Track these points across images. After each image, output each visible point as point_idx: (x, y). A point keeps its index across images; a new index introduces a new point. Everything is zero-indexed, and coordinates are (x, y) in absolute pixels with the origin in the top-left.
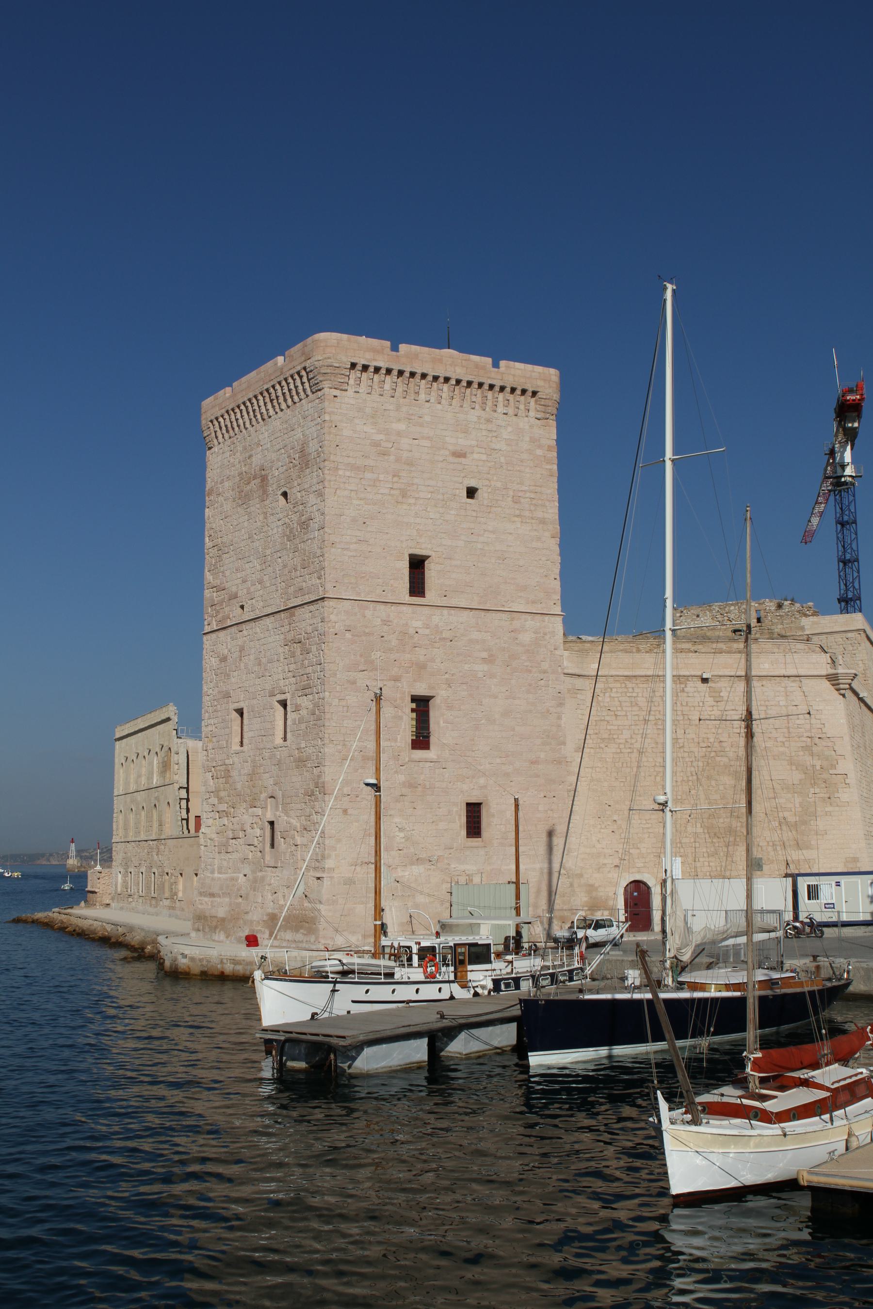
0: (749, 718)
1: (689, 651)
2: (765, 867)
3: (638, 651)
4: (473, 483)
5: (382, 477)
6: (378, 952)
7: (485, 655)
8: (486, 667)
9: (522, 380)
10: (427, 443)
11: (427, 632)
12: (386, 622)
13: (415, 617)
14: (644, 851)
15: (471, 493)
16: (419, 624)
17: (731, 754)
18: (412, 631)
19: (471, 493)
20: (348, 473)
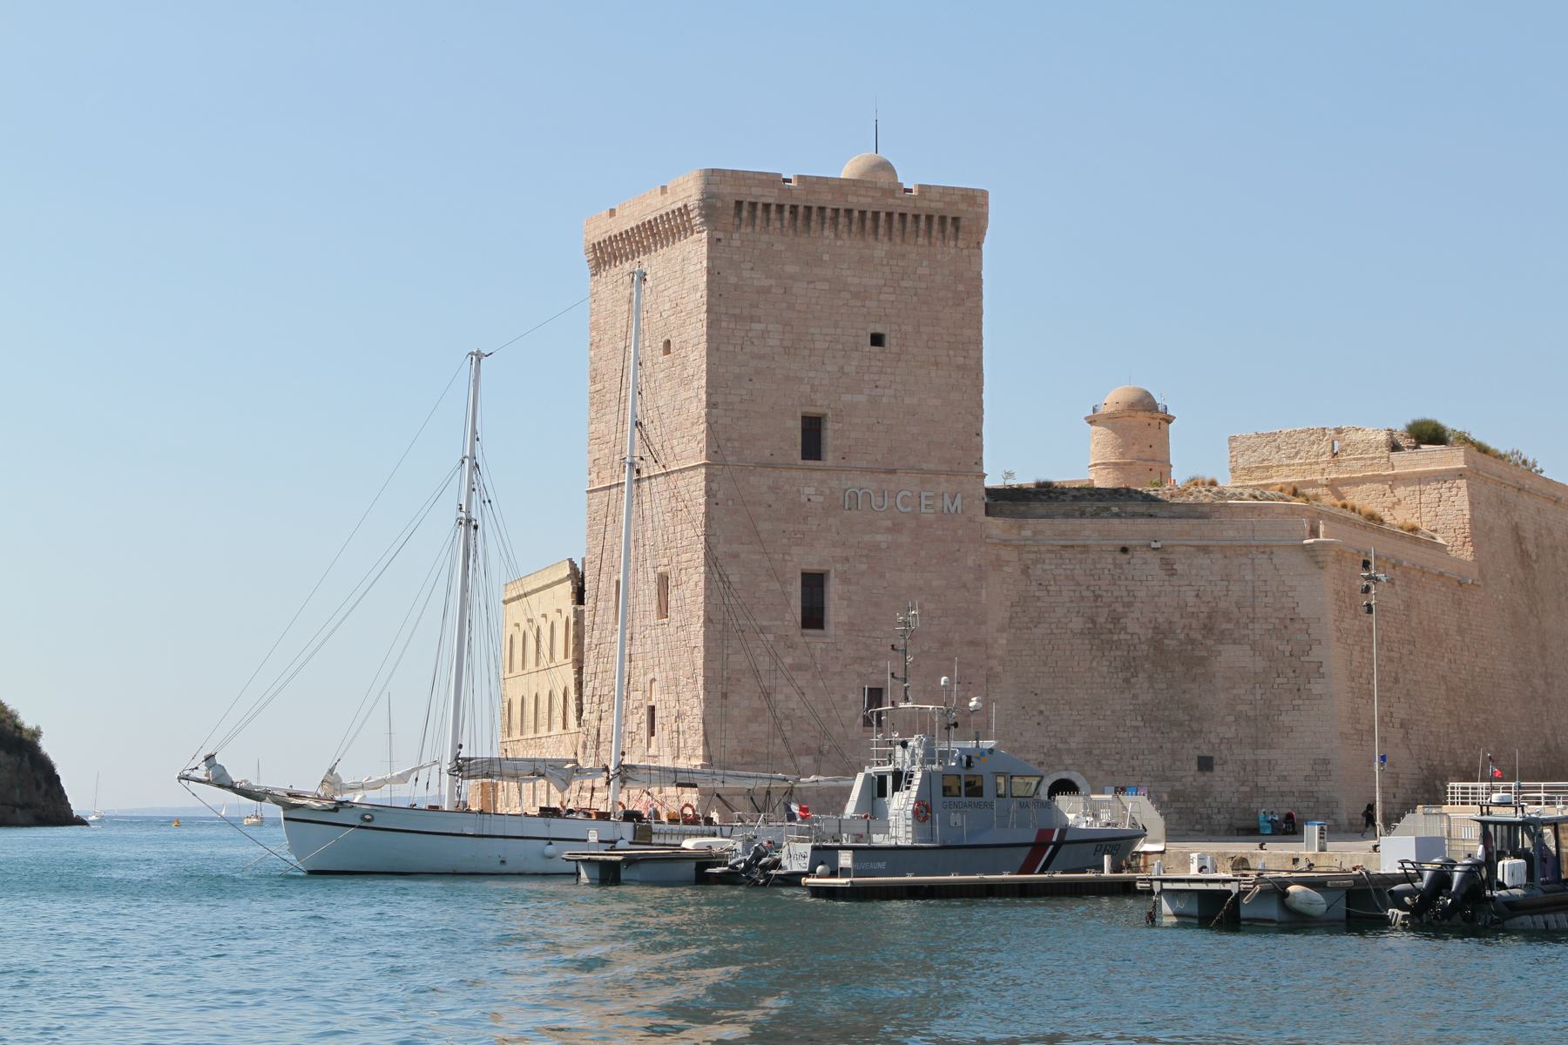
0: (525, 595)
1: (1142, 515)
2: (1216, 768)
3: (1082, 515)
4: (879, 329)
5: (770, 327)
6: (462, 768)
7: (889, 523)
8: (890, 538)
9: (940, 205)
10: (826, 286)
11: (821, 499)
12: (773, 489)
13: (810, 484)
14: (1073, 746)
15: (877, 340)
16: (809, 491)
17: (1182, 637)
18: (804, 499)
19: (877, 340)
20: (732, 325)
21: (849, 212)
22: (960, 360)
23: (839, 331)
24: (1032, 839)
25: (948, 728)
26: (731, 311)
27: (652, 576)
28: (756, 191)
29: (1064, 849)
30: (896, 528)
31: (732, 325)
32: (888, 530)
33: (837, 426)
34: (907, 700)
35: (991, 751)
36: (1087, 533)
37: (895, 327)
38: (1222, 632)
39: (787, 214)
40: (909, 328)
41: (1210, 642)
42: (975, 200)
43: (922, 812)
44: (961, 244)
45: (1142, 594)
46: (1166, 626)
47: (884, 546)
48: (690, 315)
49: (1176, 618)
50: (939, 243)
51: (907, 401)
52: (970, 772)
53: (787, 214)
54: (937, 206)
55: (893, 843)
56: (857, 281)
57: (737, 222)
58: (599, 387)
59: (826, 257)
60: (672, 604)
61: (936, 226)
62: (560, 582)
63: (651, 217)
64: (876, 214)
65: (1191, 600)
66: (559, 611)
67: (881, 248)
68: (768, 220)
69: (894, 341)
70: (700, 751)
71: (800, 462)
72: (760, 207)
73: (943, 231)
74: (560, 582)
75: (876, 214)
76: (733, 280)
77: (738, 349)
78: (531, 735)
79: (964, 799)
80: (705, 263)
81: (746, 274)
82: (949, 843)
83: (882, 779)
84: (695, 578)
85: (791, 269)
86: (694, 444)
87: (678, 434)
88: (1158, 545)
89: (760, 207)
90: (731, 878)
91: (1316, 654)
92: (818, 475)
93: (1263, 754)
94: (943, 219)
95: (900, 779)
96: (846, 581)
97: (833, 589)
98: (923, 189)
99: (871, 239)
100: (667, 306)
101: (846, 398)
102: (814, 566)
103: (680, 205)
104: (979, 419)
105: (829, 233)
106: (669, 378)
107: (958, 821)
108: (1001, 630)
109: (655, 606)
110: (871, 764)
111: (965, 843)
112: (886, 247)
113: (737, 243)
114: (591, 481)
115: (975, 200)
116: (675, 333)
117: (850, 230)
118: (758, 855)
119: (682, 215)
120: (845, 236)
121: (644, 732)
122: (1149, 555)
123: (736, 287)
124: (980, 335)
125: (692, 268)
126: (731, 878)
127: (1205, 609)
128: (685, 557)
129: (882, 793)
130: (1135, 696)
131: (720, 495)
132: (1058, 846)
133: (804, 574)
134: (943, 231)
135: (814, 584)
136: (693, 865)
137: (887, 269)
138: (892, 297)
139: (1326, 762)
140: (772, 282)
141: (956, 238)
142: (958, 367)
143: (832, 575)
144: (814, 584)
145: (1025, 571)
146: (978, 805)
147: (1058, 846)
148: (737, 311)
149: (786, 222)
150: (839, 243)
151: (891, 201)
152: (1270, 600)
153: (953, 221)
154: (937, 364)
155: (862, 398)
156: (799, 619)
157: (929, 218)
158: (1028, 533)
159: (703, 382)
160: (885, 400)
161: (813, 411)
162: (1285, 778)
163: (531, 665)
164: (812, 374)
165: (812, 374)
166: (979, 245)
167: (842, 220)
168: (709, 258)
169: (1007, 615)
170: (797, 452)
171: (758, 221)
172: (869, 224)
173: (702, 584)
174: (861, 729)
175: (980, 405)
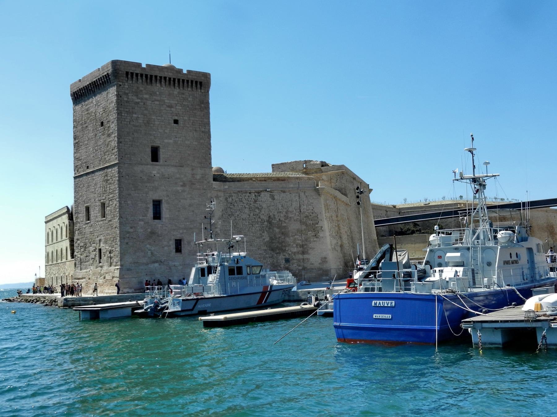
4: (176, 118)
5: (139, 116)
8: (182, 188)
9: (196, 77)
11: (158, 175)
15: (176, 122)
16: (155, 172)
18: (153, 175)
21: (165, 78)
22: (203, 129)
23: (163, 118)
24: (261, 290)
25: (229, 248)
26: (126, 110)
27: (98, 204)
28: (133, 69)
29: (272, 293)
30: (184, 185)
31: (126, 115)
32: (182, 186)
33: (163, 151)
34: (211, 238)
35: (245, 257)
36: (246, 186)
37: (181, 118)
38: (291, 218)
39: (144, 77)
40: (186, 118)
41: (287, 221)
42: (207, 76)
43: (222, 282)
44: (202, 91)
45: (264, 206)
46: (272, 216)
47: (180, 191)
48: (110, 111)
49: (276, 214)
50: (195, 90)
51: (187, 142)
52: (238, 265)
53: (144, 77)
54: (195, 78)
55: (213, 296)
56: (168, 101)
57: (126, 79)
58: (77, 141)
59: (158, 93)
60: (107, 212)
61: (194, 84)
62: (64, 214)
63: (95, 80)
64: (174, 79)
65: (280, 207)
66: (64, 223)
67: (176, 91)
68: (137, 79)
69: (181, 122)
70: (119, 263)
71: (151, 163)
72: (135, 74)
73: (196, 86)
74: (64, 214)
75: (174, 79)
76: (126, 99)
77: (128, 123)
78: (55, 263)
79: (236, 276)
80: (115, 93)
81: (130, 97)
82: (233, 294)
83: (203, 270)
84: (115, 202)
85: (147, 96)
86: (113, 156)
87: (107, 153)
88: (269, 190)
89: (135, 74)
90: (145, 315)
91: (320, 224)
92: (157, 167)
93: (306, 256)
94: (196, 82)
95: (210, 270)
96: (168, 203)
97: (150, 214)
98: (189, 71)
99: (173, 87)
100: (102, 110)
101: (166, 141)
102: (157, 198)
103: (106, 73)
104: (209, 149)
105: (158, 85)
106: (103, 135)
107: (235, 285)
108: (219, 219)
109: (100, 214)
110: (197, 264)
111: (239, 293)
112: (178, 91)
113: (127, 87)
114: (75, 174)
115: (207, 76)
116: (105, 119)
117: (165, 85)
118: (157, 305)
119: (106, 77)
120: (164, 86)
121: (97, 258)
122: (266, 193)
123: (127, 102)
124: (209, 121)
125: (111, 95)
126: (145, 315)
127: (285, 210)
128: (111, 196)
129: (203, 275)
130: (264, 239)
131: (124, 173)
132: (270, 292)
133: (154, 201)
134: (196, 86)
135: (157, 205)
136: (130, 309)
137: (178, 98)
138: (180, 108)
139: (325, 258)
140: (139, 100)
141: (201, 89)
142: (203, 132)
143: (163, 201)
144: (157, 205)
145: (226, 199)
146: (242, 278)
147: (270, 292)
148: (127, 110)
149: (144, 80)
150: (162, 88)
151: (179, 75)
152: (305, 207)
153: (199, 83)
154: (196, 131)
155: (171, 141)
156: (152, 216)
157: (192, 82)
158: (226, 187)
159: (116, 134)
160: (179, 142)
161: (155, 145)
162: (313, 264)
163: (55, 241)
164: (154, 132)
165: (154, 132)
166: (208, 91)
167: (163, 80)
168: (117, 91)
169: (221, 214)
170: (149, 159)
171: (134, 79)
172: (172, 82)
173: (118, 205)
174: (175, 253)
175: (210, 144)
